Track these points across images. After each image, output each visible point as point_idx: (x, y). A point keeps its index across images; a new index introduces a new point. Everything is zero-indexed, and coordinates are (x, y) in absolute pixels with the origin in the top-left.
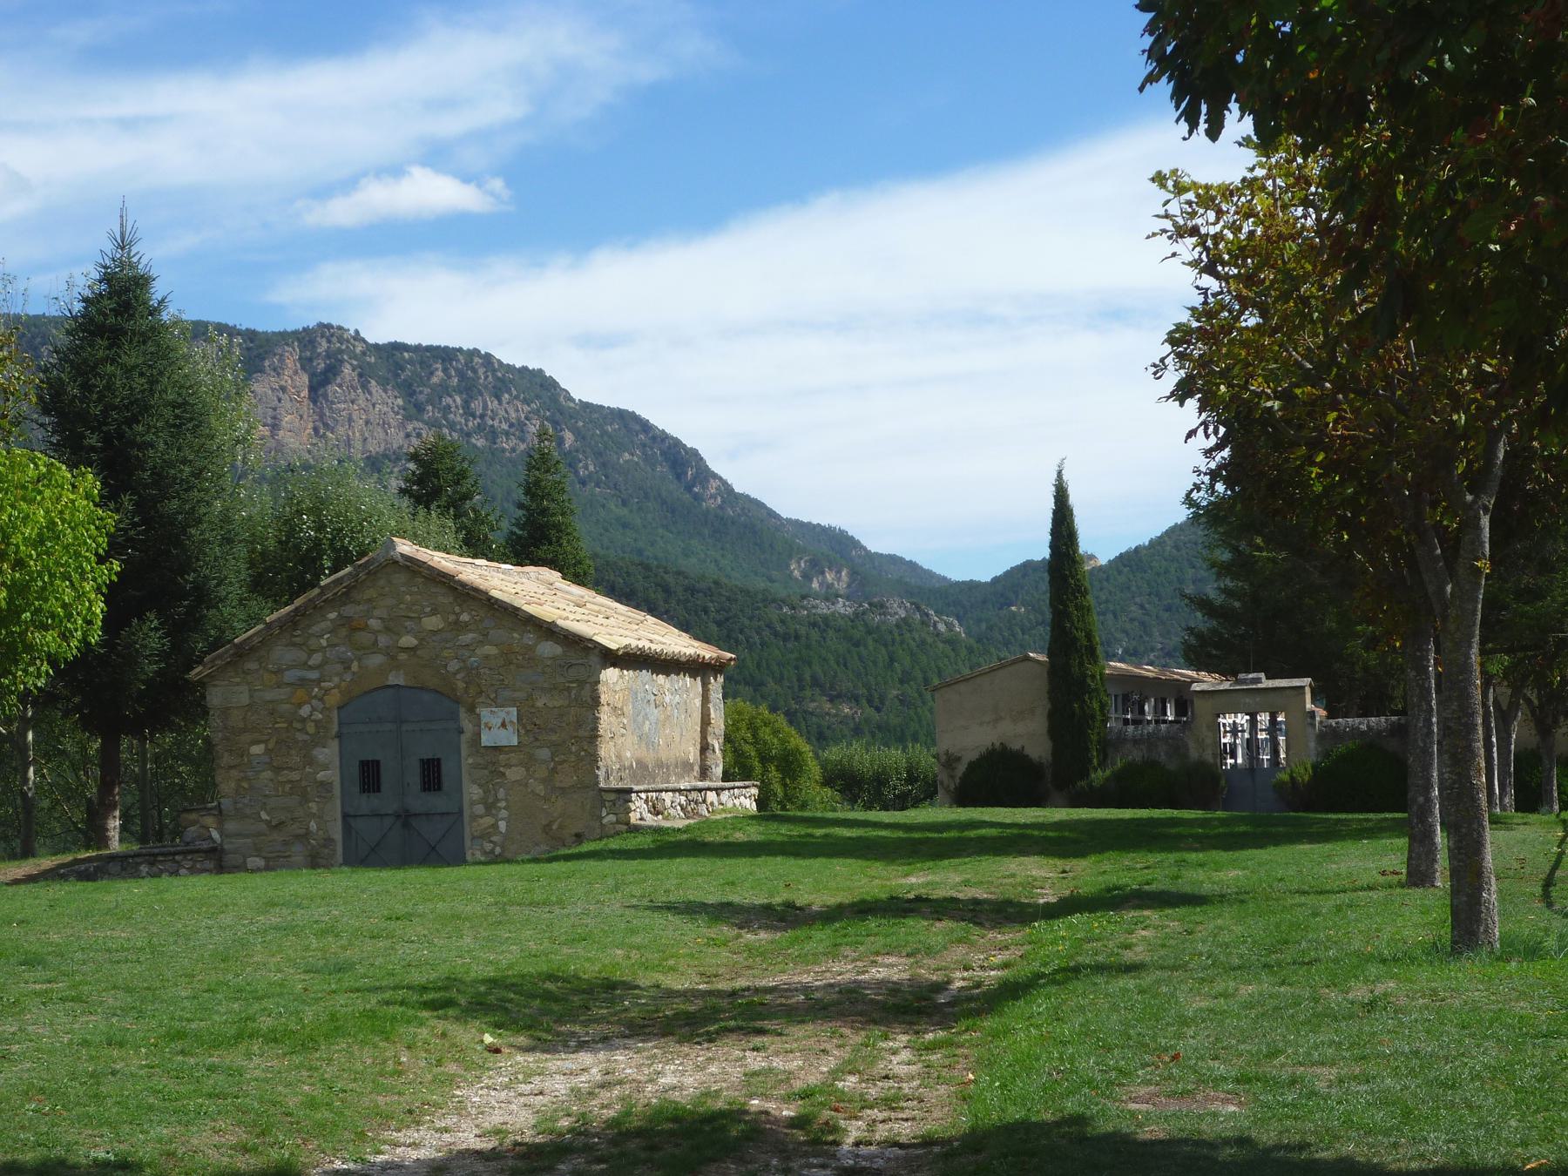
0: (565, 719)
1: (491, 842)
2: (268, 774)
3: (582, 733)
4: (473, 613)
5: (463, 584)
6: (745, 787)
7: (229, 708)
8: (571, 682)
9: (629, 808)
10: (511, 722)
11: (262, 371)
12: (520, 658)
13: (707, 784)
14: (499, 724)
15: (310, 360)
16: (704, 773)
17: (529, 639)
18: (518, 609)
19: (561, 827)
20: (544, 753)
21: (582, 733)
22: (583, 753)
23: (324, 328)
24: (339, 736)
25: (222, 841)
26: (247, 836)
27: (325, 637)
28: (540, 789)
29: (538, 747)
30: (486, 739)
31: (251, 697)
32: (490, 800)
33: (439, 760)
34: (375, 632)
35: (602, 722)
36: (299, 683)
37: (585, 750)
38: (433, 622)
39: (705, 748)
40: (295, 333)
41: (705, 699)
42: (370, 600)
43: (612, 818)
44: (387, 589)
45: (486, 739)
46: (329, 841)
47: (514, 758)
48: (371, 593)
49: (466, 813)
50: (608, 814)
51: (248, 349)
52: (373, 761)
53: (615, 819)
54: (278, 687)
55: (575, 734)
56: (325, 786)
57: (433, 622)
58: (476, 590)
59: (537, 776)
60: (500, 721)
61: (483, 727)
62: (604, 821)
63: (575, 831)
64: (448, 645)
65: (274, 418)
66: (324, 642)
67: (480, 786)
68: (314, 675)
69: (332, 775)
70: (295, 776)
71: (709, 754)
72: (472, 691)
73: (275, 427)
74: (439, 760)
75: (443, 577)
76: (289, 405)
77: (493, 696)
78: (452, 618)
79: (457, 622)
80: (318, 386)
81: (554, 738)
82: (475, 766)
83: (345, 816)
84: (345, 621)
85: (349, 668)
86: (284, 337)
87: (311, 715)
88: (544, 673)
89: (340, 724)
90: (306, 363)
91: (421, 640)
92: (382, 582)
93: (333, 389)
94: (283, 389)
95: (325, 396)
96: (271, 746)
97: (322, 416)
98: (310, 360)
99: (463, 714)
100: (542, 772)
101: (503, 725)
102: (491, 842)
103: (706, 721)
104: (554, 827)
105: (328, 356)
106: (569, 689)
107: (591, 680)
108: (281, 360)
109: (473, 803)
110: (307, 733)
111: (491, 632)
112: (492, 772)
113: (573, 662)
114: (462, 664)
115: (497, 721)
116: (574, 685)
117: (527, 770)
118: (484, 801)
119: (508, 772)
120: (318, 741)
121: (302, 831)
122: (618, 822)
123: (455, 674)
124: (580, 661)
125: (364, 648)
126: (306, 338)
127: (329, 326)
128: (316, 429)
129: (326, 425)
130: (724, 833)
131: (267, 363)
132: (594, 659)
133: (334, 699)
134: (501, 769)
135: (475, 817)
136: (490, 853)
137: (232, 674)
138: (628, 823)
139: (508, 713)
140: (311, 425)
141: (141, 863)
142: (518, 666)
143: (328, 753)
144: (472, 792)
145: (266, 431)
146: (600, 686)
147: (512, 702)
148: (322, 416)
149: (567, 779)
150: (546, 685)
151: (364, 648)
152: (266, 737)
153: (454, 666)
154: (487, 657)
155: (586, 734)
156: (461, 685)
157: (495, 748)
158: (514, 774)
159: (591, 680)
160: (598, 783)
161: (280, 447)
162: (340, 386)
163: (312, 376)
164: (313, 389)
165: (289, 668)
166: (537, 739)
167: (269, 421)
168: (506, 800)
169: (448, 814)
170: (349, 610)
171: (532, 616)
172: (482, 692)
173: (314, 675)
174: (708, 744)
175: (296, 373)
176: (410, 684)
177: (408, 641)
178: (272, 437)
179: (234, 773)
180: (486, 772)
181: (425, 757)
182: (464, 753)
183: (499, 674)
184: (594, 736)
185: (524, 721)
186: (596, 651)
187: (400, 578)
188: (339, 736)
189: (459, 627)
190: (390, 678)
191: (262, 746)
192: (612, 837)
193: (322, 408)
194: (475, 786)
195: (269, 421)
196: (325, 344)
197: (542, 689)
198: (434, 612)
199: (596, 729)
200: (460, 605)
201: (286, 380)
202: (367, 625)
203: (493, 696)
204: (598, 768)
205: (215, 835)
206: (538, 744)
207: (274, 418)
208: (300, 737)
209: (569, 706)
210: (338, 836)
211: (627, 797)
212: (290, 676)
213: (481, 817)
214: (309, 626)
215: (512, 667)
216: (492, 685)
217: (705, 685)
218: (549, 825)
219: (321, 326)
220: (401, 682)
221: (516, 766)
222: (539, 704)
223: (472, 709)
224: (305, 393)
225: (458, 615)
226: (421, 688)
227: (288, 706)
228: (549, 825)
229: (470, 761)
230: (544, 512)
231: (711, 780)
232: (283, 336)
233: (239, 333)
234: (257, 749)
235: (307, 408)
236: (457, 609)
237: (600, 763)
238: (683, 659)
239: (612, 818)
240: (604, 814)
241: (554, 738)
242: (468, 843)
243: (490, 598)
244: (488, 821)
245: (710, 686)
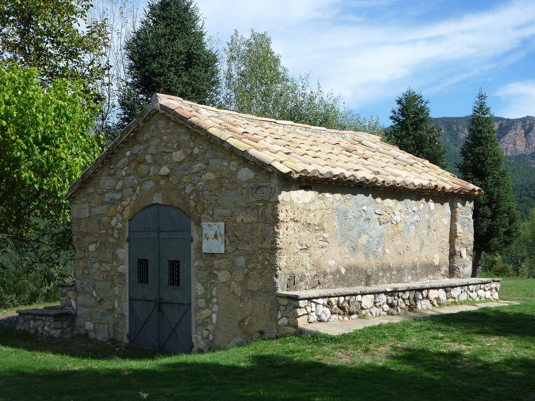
0: (255, 233)
1: (207, 330)
2: (96, 265)
3: (266, 245)
4: (201, 147)
5: (192, 124)
6: (484, 283)
7: (80, 219)
8: (258, 201)
9: (296, 313)
10: (220, 234)
11: (511, 129)
12: (227, 181)
13: (454, 281)
14: (213, 236)
15: (525, 126)
16: (452, 272)
17: (234, 165)
18: (223, 142)
19: (250, 324)
20: (241, 261)
21: (266, 245)
22: (266, 263)
23: (528, 117)
24: (129, 240)
25: (77, 309)
26: (87, 307)
27: (125, 169)
28: (238, 290)
29: (238, 256)
30: (206, 248)
31: (90, 211)
32: (208, 297)
33: (179, 262)
34: (149, 165)
35: (281, 236)
36: (111, 202)
37: (268, 260)
38: (178, 156)
39: (452, 254)
40: (520, 119)
41: (453, 219)
42: (146, 141)
43: (284, 321)
44: (155, 132)
45: (206, 248)
46: (123, 315)
47: (223, 263)
48: (147, 136)
49: (193, 305)
50: (282, 317)
51: (507, 124)
52: (145, 260)
53: (286, 322)
54: (102, 205)
55: (261, 246)
56: (121, 275)
57: (178, 156)
58: (200, 128)
59: (236, 279)
60: (214, 233)
61: (204, 237)
62: (280, 322)
63: (260, 328)
64: (186, 173)
65: (514, 142)
66: (124, 173)
67: (203, 284)
68: (118, 196)
69: (124, 268)
70: (108, 268)
71: (457, 259)
72: (199, 209)
73: (515, 144)
74: (179, 262)
75: (182, 120)
76: (519, 138)
77: (211, 213)
78: (189, 151)
79: (191, 155)
80: (526, 133)
81: (247, 248)
82: (199, 268)
83: (131, 299)
84: (135, 156)
85: (135, 191)
86: (517, 120)
87: (116, 225)
88: (242, 194)
89: (130, 231)
90: (523, 127)
91: (172, 169)
92: (152, 127)
93: (531, 134)
94: (517, 134)
95: (529, 136)
96: (98, 246)
97: (528, 141)
98: (525, 126)
99: (193, 227)
100: (240, 277)
101: (216, 236)
102: (207, 330)
103: (453, 235)
104: (246, 323)
105: (529, 125)
106: (257, 207)
107: (272, 200)
108: (517, 126)
109: (197, 298)
110: (114, 238)
111: (211, 161)
112: (209, 274)
113: (261, 184)
114: (194, 187)
115: (211, 233)
116: (261, 204)
117: (231, 274)
118: (204, 296)
119: (219, 275)
120: (118, 245)
121: (110, 307)
122: (289, 325)
123: (190, 195)
124: (265, 184)
125: (143, 177)
126: (523, 120)
127: (530, 117)
128: (526, 145)
129: (529, 144)
130: (318, 357)
131: (512, 127)
132: (275, 182)
133: (127, 214)
134: (215, 272)
135: (198, 309)
136: (206, 338)
137: (83, 196)
138: (296, 326)
139: (218, 227)
140: (525, 144)
141: (30, 319)
142: (227, 189)
143: (123, 253)
144: (198, 288)
145: (512, 146)
146: (279, 206)
147: (222, 218)
148: (528, 141)
149: (254, 285)
150: (243, 204)
151: (143, 177)
152: (95, 240)
153: (189, 189)
154: (208, 181)
155: (268, 246)
156: (192, 204)
157: (212, 255)
158: (223, 276)
159: (272, 200)
160: (275, 289)
161: (516, 150)
162: (533, 133)
163: (525, 130)
164: (525, 134)
165: (108, 191)
166: (237, 249)
167: (513, 143)
168: (217, 297)
169: (183, 304)
170: (137, 149)
171: (232, 147)
172: (205, 209)
173: (118, 196)
174: (455, 250)
175: (520, 130)
176: (166, 203)
177: (165, 170)
178: (514, 147)
179: (81, 263)
180: (206, 273)
181: (172, 259)
182: (193, 257)
183: (215, 195)
184: (274, 249)
185: (229, 234)
186: (275, 175)
187: (162, 123)
188: (129, 240)
189: (192, 158)
190: (154, 198)
191: (94, 245)
192: (273, 339)
193: (528, 139)
194: (199, 284)
195: (513, 143)
196: (529, 122)
197: (241, 207)
198: (179, 148)
199: (274, 242)
200: (193, 141)
201: (518, 132)
202: (145, 160)
203: (211, 213)
204: (277, 276)
205: (73, 303)
206: (237, 253)
207: (514, 142)
208: (111, 240)
209: (257, 222)
210: (127, 313)
211: (295, 303)
212: (108, 197)
213: (203, 309)
214: (117, 161)
215: (223, 189)
216: (211, 204)
217: (453, 208)
218: (242, 321)
219: (528, 117)
220: (160, 202)
221: (224, 270)
222: (239, 220)
223: (198, 223)
224: (523, 135)
225: (192, 148)
226: (171, 206)
227: (106, 218)
228: (242, 321)
229: (196, 264)
230: (480, 132)
231: (459, 277)
232: (517, 120)
233: (505, 119)
234: (92, 248)
235: (524, 139)
236: (192, 145)
237: (279, 272)
238: (411, 187)
239: (284, 321)
240: (279, 317)
241: (247, 248)
242: (193, 329)
243: (208, 134)
244: (207, 312)
245: (458, 210)
